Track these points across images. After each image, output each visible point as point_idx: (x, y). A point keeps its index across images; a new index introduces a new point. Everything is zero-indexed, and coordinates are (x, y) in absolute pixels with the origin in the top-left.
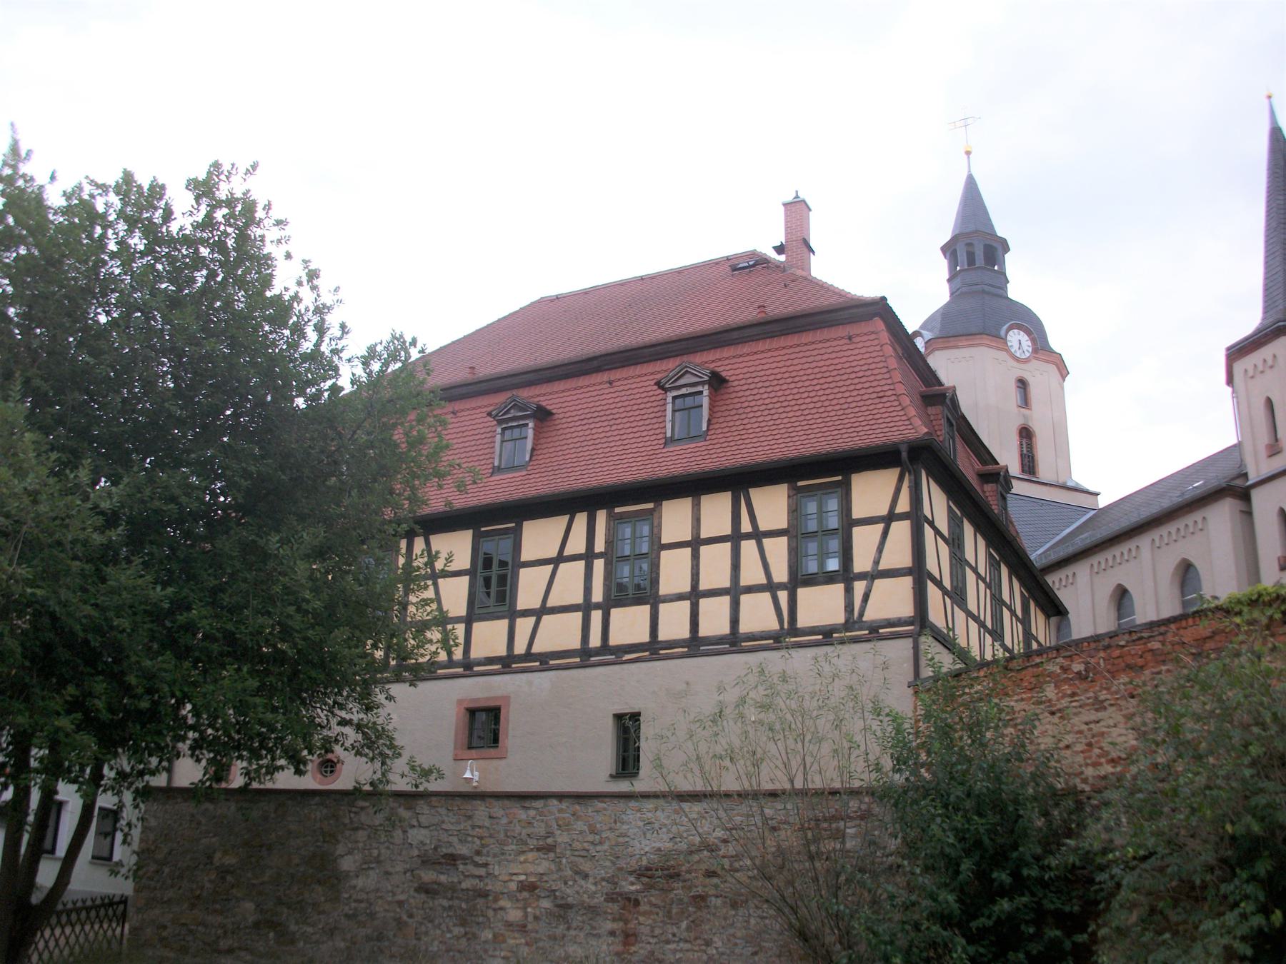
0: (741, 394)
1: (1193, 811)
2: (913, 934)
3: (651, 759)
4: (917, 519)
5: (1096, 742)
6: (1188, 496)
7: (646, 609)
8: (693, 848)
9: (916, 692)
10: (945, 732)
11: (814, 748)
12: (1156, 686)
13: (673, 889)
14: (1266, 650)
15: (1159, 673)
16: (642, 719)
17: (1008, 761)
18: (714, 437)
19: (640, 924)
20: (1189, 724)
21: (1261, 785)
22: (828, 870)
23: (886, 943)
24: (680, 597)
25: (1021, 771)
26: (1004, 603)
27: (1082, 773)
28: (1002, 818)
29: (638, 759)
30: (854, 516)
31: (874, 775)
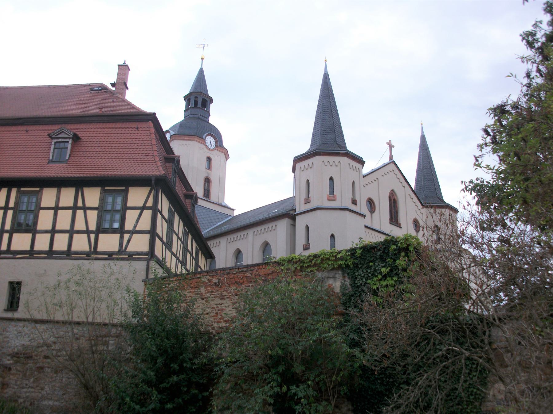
0: (86, 145)
1: (256, 344)
2: (135, 389)
3: (24, 303)
4: (155, 210)
5: (220, 313)
6: (271, 215)
7: (30, 235)
8: (39, 345)
9: (145, 284)
10: (156, 302)
11: (98, 304)
12: (247, 292)
13: (28, 364)
14: (292, 281)
15: (249, 286)
16: (22, 284)
17: (182, 317)
18: (71, 162)
19: (10, 379)
20: (258, 308)
21: (284, 335)
22: (100, 359)
23: (123, 392)
24: (46, 232)
25: (187, 322)
26: (188, 251)
27: (213, 325)
28: (177, 342)
29: (18, 303)
30: (128, 205)
31: (123, 318)
